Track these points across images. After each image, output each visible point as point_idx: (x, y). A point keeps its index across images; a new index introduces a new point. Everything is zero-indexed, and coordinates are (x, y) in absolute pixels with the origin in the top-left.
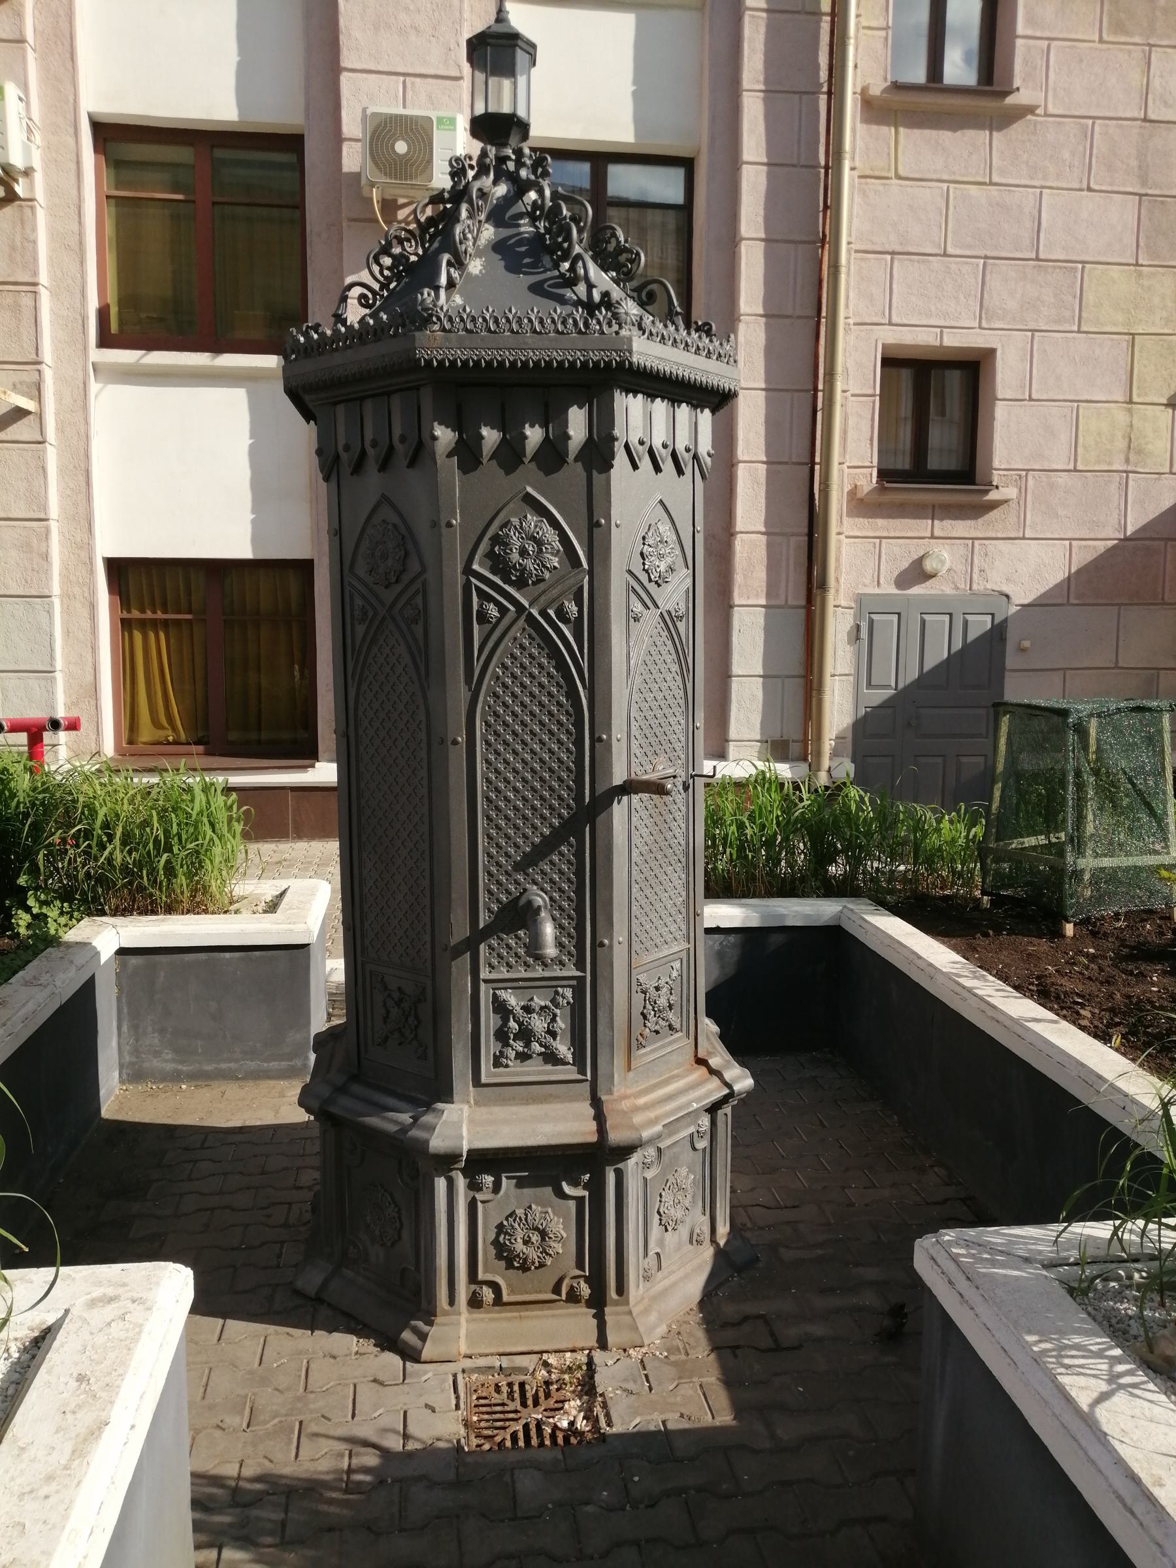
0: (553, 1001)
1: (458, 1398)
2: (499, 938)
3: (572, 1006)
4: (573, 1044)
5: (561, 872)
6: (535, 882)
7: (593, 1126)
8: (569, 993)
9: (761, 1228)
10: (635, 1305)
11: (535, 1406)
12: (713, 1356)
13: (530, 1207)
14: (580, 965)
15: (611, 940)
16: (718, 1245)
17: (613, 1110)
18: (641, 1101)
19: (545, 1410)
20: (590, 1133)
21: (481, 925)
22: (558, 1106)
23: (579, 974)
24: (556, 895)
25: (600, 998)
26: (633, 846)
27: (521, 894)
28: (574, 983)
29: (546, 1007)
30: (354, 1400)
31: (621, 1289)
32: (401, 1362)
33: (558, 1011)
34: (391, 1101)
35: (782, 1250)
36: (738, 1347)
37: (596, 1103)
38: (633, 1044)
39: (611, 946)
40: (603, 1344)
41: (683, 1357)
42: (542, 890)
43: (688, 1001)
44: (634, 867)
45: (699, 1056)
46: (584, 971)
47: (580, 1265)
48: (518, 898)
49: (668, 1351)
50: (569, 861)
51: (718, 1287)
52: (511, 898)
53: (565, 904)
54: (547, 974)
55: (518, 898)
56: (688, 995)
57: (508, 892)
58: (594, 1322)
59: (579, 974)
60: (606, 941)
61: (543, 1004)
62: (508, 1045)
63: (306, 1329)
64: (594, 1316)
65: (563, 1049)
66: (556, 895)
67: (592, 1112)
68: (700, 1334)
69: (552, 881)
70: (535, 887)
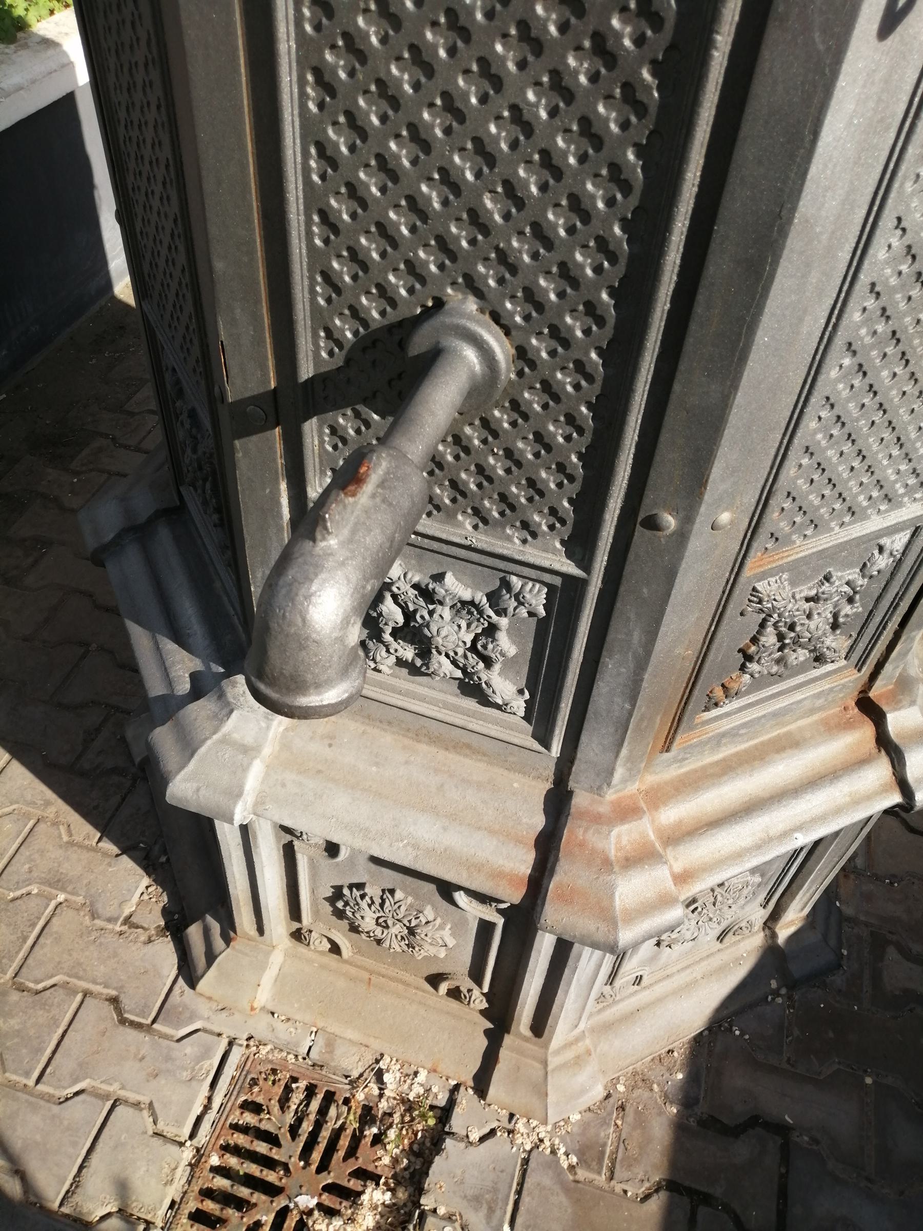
0: (493, 598)
1: (207, 1108)
2: (357, 415)
3: (542, 625)
4: (532, 683)
5: (567, 274)
6: (473, 286)
7: (523, 862)
8: (537, 599)
9: (878, 878)
10: (557, 1052)
11: (319, 1170)
12: (655, 1205)
13: (392, 892)
14: (580, 545)
15: (687, 520)
16: (774, 935)
17: (582, 845)
18: (673, 814)
19: (328, 1188)
20: (512, 879)
21: (306, 371)
22: (482, 766)
23: (570, 568)
24: (539, 347)
25: (616, 633)
26: (839, 341)
27: (428, 313)
28: (558, 581)
29: (472, 603)
30: (65, 1032)
31: (539, 1025)
32: (174, 972)
33: (504, 622)
34: (188, 611)
35: (892, 953)
36: (706, 1199)
37: (558, 803)
38: (696, 691)
39: (682, 536)
40: (481, 1084)
41: (601, 1179)
42: (496, 317)
43: (894, 606)
44: (861, 298)
45: (872, 694)
46: (586, 565)
47: (476, 974)
48: (415, 322)
49: (581, 1154)
50: (604, 245)
51: (739, 1012)
52: (393, 315)
53: (565, 380)
54: (482, 540)
55: (415, 322)
56: (899, 597)
57: (385, 294)
58: (482, 1043)
59: (570, 568)
60: (670, 521)
61: (467, 595)
62: (380, 640)
63: (96, 826)
64: (487, 1032)
65: (505, 686)
66: (539, 347)
67: (539, 821)
68: (660, 1131)
69: (532, 297)
70: (472, 305)
